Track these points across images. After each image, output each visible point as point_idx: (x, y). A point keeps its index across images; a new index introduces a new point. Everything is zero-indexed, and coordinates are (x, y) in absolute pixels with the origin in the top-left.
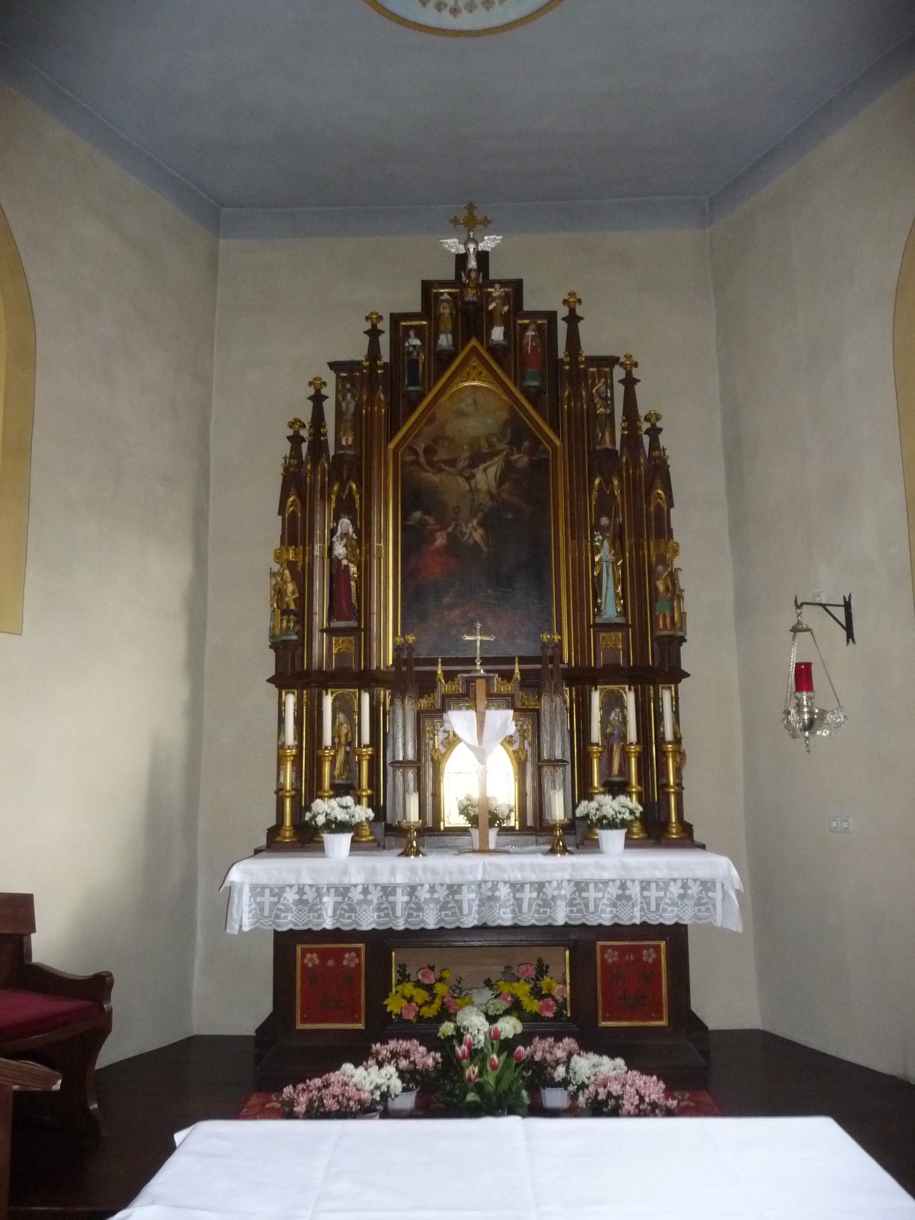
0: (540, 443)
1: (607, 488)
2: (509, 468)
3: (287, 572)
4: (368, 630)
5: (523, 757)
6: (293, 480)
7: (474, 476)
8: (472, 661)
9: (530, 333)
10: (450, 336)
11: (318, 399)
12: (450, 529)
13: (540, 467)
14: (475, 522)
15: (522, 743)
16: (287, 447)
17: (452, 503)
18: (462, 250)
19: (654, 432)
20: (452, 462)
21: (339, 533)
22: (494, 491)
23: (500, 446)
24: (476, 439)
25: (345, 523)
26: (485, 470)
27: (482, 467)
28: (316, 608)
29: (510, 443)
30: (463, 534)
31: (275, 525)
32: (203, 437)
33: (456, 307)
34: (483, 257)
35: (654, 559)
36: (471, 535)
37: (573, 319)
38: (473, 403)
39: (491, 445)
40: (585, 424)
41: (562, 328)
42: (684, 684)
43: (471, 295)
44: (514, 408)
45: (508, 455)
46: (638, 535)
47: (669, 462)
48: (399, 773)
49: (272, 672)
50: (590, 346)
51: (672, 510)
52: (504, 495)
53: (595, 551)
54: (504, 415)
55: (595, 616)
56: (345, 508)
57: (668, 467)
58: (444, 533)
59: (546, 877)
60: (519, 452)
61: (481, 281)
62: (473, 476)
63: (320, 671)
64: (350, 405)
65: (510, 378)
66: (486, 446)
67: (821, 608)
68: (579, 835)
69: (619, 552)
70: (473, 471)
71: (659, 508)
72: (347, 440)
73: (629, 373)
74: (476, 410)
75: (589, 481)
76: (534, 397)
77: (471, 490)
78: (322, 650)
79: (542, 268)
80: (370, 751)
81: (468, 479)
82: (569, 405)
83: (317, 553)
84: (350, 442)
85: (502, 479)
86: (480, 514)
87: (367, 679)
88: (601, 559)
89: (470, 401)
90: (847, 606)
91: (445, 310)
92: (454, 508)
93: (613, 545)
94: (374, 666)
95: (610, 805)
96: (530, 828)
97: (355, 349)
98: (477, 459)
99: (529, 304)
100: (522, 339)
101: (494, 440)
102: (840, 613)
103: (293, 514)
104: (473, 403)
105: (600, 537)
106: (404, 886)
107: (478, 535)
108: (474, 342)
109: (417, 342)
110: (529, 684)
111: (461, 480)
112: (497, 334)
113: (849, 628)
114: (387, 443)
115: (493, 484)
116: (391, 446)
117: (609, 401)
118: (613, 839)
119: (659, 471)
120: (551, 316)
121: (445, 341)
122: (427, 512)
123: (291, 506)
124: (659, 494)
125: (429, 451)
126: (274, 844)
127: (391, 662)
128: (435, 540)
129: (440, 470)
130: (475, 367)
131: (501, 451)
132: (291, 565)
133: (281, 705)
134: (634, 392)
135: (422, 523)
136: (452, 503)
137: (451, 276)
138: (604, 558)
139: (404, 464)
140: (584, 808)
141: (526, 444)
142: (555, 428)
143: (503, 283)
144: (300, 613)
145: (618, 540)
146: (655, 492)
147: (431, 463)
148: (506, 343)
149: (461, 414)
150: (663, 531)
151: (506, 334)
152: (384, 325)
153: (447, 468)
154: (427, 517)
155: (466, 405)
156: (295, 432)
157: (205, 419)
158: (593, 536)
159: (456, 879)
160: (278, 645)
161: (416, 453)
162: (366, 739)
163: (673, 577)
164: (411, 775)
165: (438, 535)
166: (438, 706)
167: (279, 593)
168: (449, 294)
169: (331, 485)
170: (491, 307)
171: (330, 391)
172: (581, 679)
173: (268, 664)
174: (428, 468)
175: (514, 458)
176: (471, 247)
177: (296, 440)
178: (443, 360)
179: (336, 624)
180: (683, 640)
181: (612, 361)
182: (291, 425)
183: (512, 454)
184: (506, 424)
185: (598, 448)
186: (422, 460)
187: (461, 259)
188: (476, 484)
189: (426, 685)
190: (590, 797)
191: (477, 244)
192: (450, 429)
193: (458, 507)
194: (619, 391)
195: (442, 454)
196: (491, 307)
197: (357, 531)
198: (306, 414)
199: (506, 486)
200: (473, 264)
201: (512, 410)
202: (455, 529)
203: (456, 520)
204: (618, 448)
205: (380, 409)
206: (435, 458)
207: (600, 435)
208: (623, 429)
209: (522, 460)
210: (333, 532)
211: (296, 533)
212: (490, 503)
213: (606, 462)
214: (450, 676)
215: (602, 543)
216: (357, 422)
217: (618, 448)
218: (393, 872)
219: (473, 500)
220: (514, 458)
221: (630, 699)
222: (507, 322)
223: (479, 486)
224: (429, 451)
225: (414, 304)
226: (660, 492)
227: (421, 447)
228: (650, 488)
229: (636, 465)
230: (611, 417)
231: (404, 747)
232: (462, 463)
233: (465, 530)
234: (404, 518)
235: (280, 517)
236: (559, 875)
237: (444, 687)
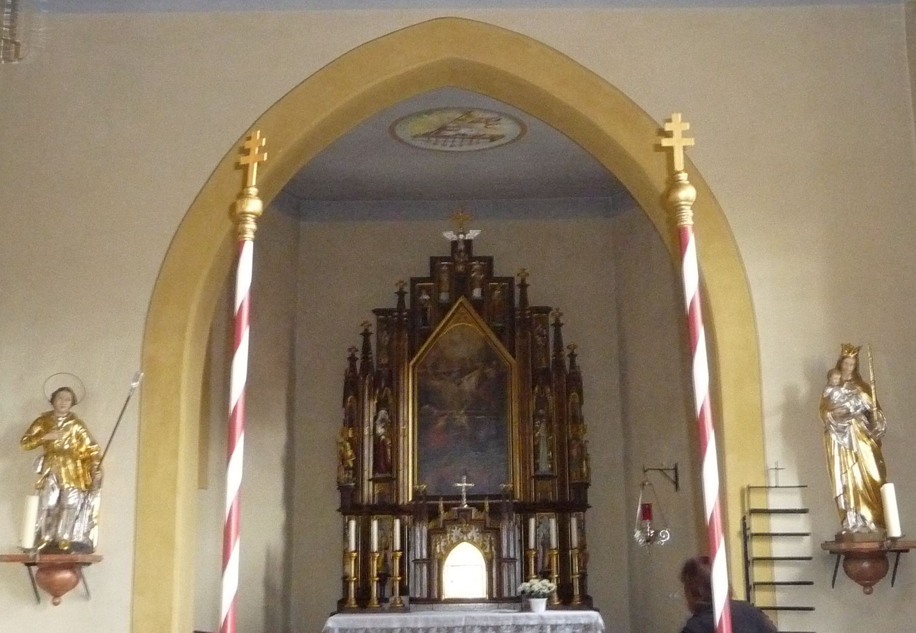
2: (483, 378)
3: (348, 444)
4: (397, 479)
5: (490, 557)
6: (351, 386)
8: (459, 497)
9: (497, 292)
11: (366, 335)
13: (502, 377)
14: (463, 411)
15: (491, 549)
16: (346, 365)
18: (455, 238)
19: (572, 356)
21: (379, 418)
24: (463, 359)
27: (466, 377)
28: (366, 467)
31: (341, 414)
32: (292, 357)
34: (468, 243)
37: (523, 286)
38: (461, 334)
41: (517, 291)
42: (588, 510)
43: (460, 268)
46: (561, 421)
48: (512, 555)
49: (338, 506)
55: (535, 470)
59: (500, 623)
63: (368, 505)
64: (386, 339)
67: (659, 473)
68: (522, 601)
69: (550, 431)
76: (499, 333)
78: (369, 491)
79: (507, 246)
80: (399, 554)
83: (366, 433)
85: (479, 386)
87: (396, 510)
90: (676, 469)
91: (445, 278)
94: (401, 502)
95: (537, 584)
96: (495, 599)
98: (464, 372)
99: (498, 272)
102: (671, 474)
103: (351, 407)
104: (461, 334)
106: (423, 629)
109: (426, 297)
110: (492, 515)
112: (477, 293)
113: (676, 483)
114: (409, 362)
116: (412, 363)
118: (539, 605)
119: (574, 381)
120: (510, 280)
121: (444, 297)
125: (435, 366)
126: (342, 607)
127: (410, 499)
132: (350, 440)
133: (346, 528)
140: (526, 585)
142: (512, 352)
143: (480, 259)
144: (357, 469)
150: (577, 420)
151: (483, 293)
152: (407, 289)
157: (292, 339)
159: (451, 624)
160: (342, 488)
162: (397, 546)
163: (582, 448)
164: (425, 568)
166: (441, 526)
167: (343, 459)
168: (447, 265)
169: (375, 390)
171: (373, 329)
172: (526, 510)
173: (336, 499)
176: (461, 236)
177: (352, 359)
178: (444, 309)
179: (378, 475)
180: (587, 485)
181: (547, 310)
182: (350, 350)
187: (455, 244)
189: (433, 514)
190: (527, 581)
191: (465, 235)
195: (443, 368)
197: (391, 417)
198: (359, 343)
200: (461, 247)
209: (491, 372)
211: (353, 420)
214: (447, 508)
218: (416, 621)
221: (553, 523)
222: (482, 285)
225: (425, 272)
230: (546, 347)
231: (420, 550)
234: (419, 409)
236: (506, 623)
237: (443, 515)
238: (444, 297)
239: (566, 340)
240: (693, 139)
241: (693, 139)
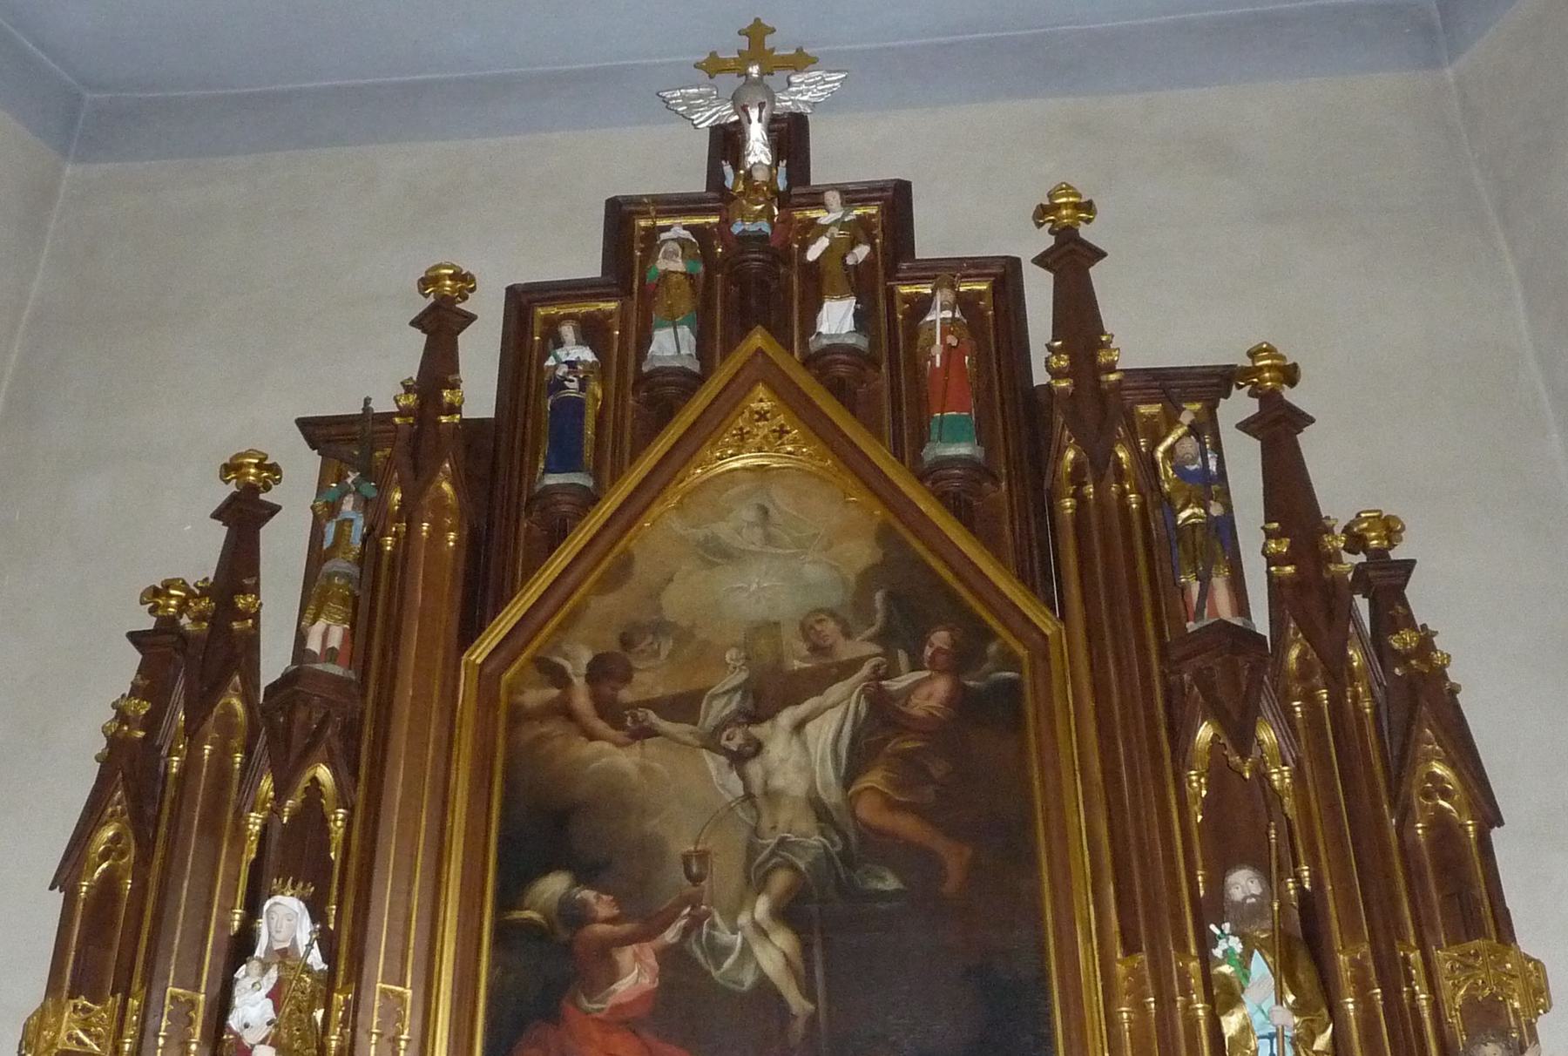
0: (990, 635)
1: (1244, 757)
7: (758, 748)
10: (685, 332)
11: (245, 514)
12: (670, 936)
13: (992, 711)
14: (762, 906)
17: (681, 844)
20: (684, 706)
22: (832, 796)
23: (847, 650)
24: (771, 628)
25: (287, 919)
26: (799, 727)
27: (787, 717)
29: (885, 638)
30: (718, 952)
33: (706, 255)
35: (1455, 1020)
36: (746, 950)
37: (1072, 259)
38: (757, 535)
39: (817, 649)
40: (1138, 560)
41: (1039, 291)
44: (897, 525)
45: (877, 676)
47: (1453, 674)
50: (1138, 337)
51: (1496, 834)
52: (868, 810)
53: (1224, 996)
54: (861, 553)
56: (297, 856)
57: (1454, 691)
58: (648, 951)
60: (915, 666)
61: (782, 184)
62: (757, 748)
65: (879, 436)
66: (802, 648)
70: (755, 731)
71: (1443, 828)
72: (329, 633)
73: (1269, 399)
74: (769, 539)
75: (1171, 729)
77: (749, 795)
81: (738, 760)
82: (1079, 496)
84: (335, 641)
85: (859, 755)
86: (781, 880)
88: (1246, 1029)
89: (748, 514)
92: (686, 859)
93: (1285, 972)
97: (380, 377)
98: (769, 694)
99: (928, 243)
100: (913, 333)
101: (830, 627)
103: (109, 883)
104: (757, 535)
105: (1236, 944)
107: (774, 955)
108: (758, 339)
111: (714, 763)
112: (836, 318)
115: (827, 777)
116: (479, 653)
117: (1212, 485)
119: (1423, 696)
120: (1006, 275)
122: (586, 874)
123: (105, 856)
124: (1433, 777)
128: (614, 975)
129: (644, 733)
130: (762, 416)
131: (852, 667)
134: (1297, 448)
135: (573, 915)
136: (681, 844)
137: (697, 184)
138: (1260, 1025)
139: (517, 716)
141: (940, 638)
142: (1038, 574)
143: (851, 196)
145: (1303, 951)
146: (1421, 772)
147: (609, 711)
148: (862, 342)
149: (717, 554)
153: (665, 726)
154: (589, 895)
155: (736, 524)
156: (161, 621)
158: (1206, 942)
161: (559, 677)
165: (625, 956)
170: (813, 254)
174: (600, 726)
175: (895, 685)
183: (892, 673)
184: (868, 579)
185: (1191, 626)
186: (582, 700)
188: (768, 774)
192: (676, 603)
193: (703, 856)
194: (1244, 463)
195: (650, 680)
196: (813, 254)
199: (874, 779)
200: (758, 149)
201: (885, 536)
202: (686, 932)
203: (694, 901)
204: (1261, 623)
205: (438, 532)
206: (626, 695)
207: (1195, 588)
208: (1272, 559)
209: (926, 692)
210: (241, 947)
212: (816, 840)
213: (1233, 670)
215: (1245, 961)
216: (367, 588)
217: (1261, 623)
219: (756, 831)
220: (895, 685)
222: (865, 286)
223: (778, 782)
224: (604, 671)
225: (587, 263)
226: (1439, 769)
227: (576, 662)
228: (1401, 764)
229: (1338, 674)
230: (1223, 531)
232: (717, 709)
233: (724, 936)
235: (58, 897)
238: (671, 345)
239: (1339, 495)
240: (489, 413)
241: (489, 413)
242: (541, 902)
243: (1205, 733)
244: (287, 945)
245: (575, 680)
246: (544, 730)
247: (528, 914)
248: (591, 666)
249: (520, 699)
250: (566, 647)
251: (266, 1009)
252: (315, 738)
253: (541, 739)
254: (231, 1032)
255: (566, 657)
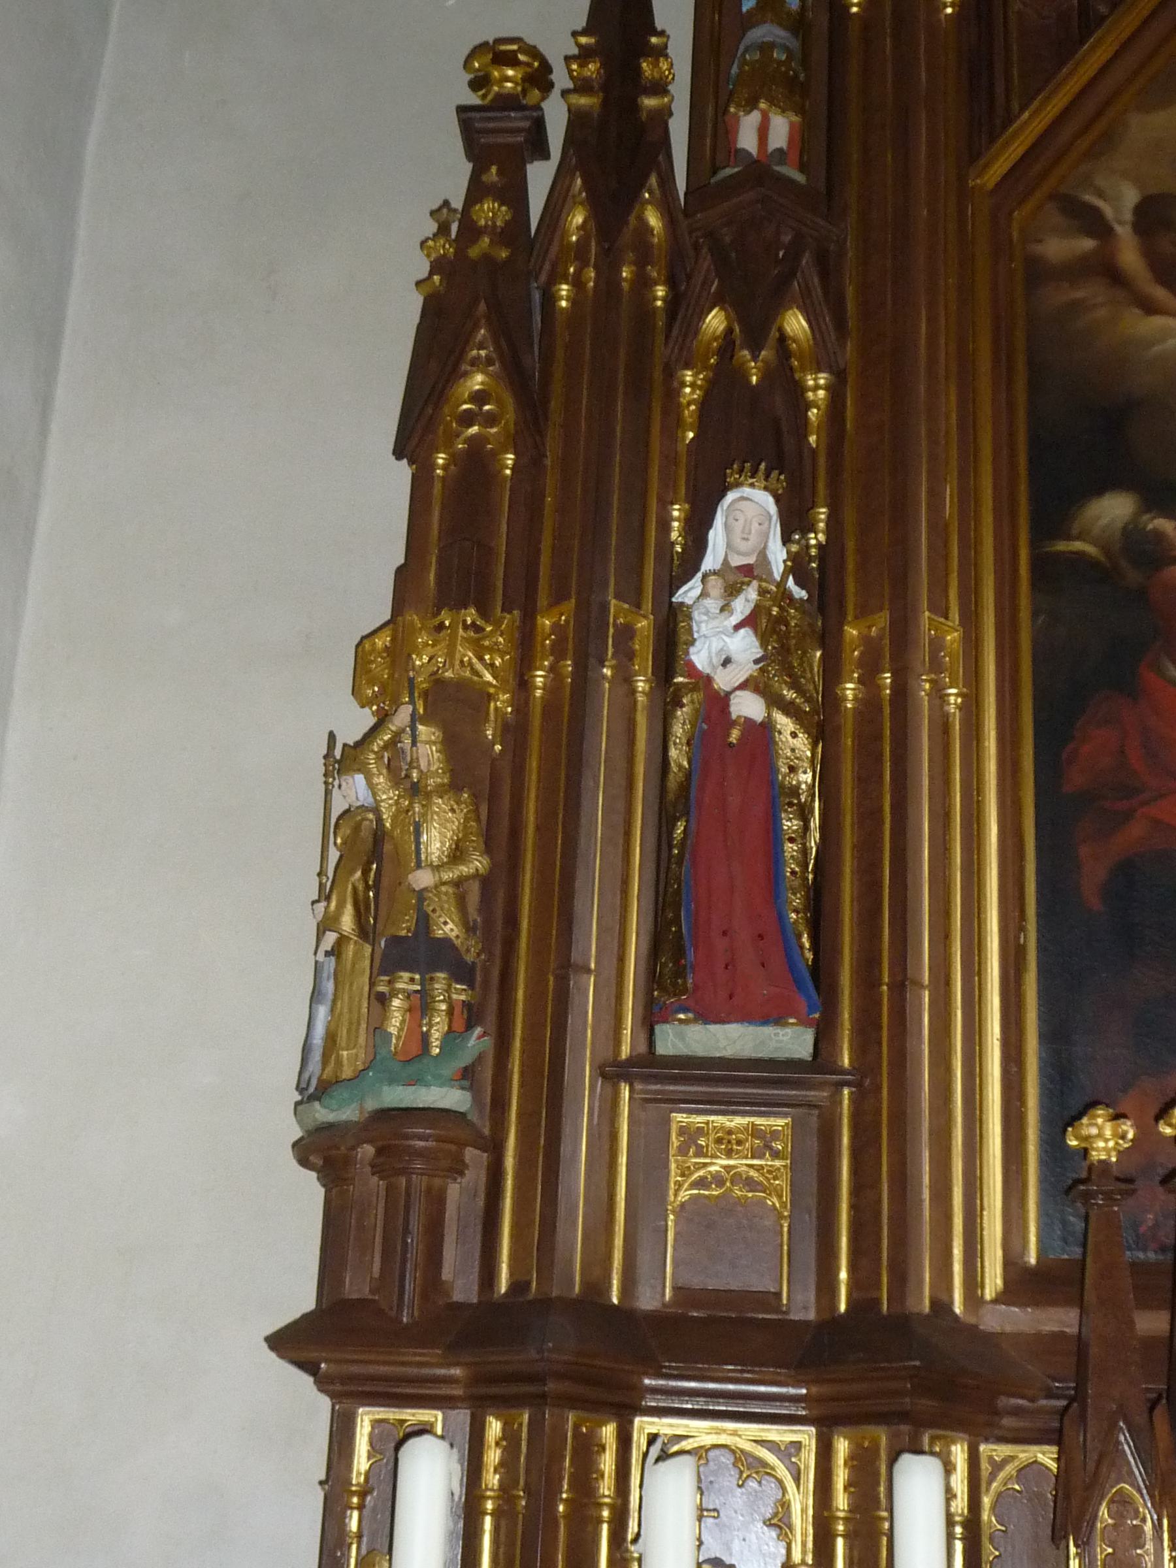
174: (1160, 293)
186: (1130, 256)
242: (1096, 531)
243: (715, 321)
244: (751, 560)
245: (1119, 229)
246: (1079, 294)
247: (1078, 546)
248: (1140, 210)
249: (1039, 249)
250: (1100, 181)
251: (745, 648)
252: (784, 281)
253: (1075, 307)
254: (691, 670)
255: (1101, 194)
